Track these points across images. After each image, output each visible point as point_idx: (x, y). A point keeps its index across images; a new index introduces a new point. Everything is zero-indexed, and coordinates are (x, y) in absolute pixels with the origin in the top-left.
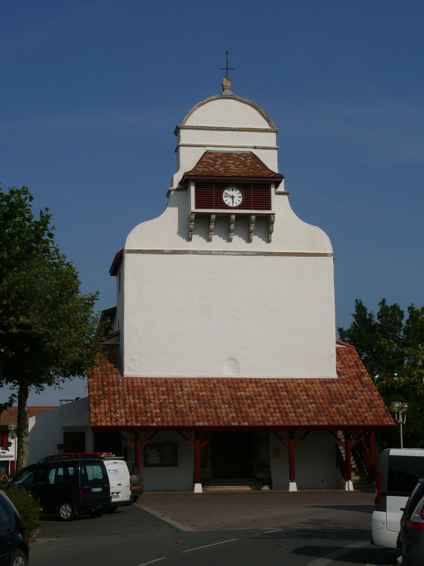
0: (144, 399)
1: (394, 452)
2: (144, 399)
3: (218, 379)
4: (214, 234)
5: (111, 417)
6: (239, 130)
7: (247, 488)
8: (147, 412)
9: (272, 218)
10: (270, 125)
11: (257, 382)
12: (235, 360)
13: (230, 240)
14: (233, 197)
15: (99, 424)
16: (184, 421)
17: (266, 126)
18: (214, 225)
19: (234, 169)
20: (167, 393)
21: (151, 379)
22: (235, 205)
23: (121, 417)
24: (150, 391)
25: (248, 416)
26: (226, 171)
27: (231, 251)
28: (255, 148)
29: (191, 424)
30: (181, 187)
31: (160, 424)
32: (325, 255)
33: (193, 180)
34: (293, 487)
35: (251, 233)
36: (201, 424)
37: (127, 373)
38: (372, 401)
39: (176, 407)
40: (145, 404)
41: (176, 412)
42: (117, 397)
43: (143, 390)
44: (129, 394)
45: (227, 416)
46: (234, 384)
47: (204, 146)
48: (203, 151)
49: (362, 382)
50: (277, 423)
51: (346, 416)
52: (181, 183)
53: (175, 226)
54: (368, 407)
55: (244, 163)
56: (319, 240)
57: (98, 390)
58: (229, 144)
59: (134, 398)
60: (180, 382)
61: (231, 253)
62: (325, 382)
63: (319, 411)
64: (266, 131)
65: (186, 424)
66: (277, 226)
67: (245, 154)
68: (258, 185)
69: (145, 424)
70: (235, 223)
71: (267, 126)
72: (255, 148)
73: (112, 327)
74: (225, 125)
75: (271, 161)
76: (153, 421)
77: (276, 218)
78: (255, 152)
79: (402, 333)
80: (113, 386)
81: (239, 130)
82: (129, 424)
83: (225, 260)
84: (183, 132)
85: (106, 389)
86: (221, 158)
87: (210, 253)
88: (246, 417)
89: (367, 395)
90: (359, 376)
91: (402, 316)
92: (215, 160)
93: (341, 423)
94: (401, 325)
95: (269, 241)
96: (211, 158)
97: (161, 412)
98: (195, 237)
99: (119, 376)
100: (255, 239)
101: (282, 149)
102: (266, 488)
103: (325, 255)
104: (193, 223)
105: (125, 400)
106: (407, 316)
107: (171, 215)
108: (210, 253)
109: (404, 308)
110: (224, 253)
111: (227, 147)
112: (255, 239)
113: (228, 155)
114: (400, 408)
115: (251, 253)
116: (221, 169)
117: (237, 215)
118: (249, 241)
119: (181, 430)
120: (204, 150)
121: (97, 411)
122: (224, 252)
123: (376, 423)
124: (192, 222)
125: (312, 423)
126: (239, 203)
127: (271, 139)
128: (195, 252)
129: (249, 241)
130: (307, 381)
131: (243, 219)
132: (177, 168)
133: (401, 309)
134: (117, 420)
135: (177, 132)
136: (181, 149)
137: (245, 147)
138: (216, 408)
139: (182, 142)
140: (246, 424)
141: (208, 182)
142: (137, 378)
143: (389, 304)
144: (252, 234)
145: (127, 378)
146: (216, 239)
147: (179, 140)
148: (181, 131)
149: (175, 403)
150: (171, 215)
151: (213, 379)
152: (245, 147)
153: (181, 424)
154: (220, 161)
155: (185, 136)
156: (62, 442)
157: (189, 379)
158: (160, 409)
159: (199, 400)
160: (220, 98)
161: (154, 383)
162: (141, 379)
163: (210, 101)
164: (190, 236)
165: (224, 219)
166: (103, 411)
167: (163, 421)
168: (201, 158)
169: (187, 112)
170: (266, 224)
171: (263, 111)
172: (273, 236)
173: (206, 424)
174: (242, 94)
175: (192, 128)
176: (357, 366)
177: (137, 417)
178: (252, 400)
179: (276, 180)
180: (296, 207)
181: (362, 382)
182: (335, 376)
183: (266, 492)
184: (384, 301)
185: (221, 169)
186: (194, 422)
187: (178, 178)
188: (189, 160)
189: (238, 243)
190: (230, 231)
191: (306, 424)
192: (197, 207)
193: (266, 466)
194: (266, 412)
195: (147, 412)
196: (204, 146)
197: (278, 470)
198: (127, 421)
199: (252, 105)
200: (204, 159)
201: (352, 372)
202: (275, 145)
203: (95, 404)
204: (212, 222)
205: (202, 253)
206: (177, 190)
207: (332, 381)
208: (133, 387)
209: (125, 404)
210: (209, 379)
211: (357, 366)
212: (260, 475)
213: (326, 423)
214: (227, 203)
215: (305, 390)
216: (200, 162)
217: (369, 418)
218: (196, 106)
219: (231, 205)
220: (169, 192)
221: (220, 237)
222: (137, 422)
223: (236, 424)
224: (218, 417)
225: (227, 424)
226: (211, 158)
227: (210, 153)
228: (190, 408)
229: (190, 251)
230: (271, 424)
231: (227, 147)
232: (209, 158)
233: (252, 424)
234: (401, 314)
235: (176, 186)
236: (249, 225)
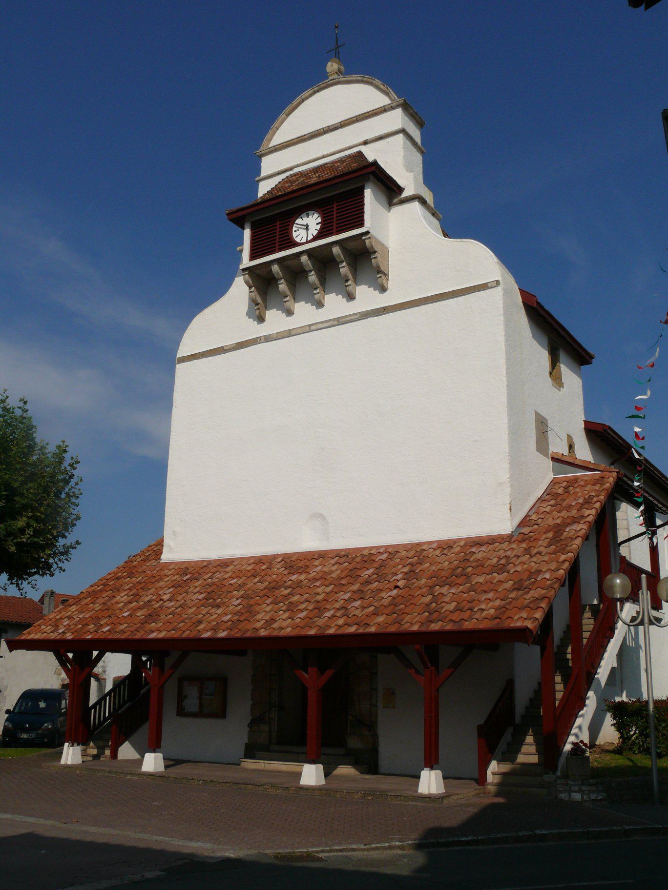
10: (387, 94)
12: (321, 517)
27: (320, 323)
64: (384, 110)
71: (384, 101)
83: (323, 336)
87: (268, 339)
95: (383, 289)
107: (240, 290)
108: (268, 339)
110: (289, 334)
111: (323, 157)
115: (353, 317)
122: (310, 326)
131: (324, 261)
137: (350, 148)
152: (350, 148)
156: (12, 709)
163: (303, 101)
174: (358, 69)
189: (334, 304)
197: (398, 736)
218: (282, 116)
221: (375, 290)
229: (259, 338)
231: (323, 157)
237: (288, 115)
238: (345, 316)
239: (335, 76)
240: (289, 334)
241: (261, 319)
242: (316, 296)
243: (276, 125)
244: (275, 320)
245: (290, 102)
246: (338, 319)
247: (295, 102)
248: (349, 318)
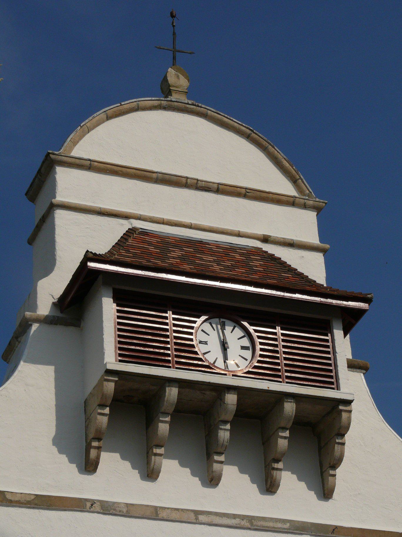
4: (168, 456)
9: (344, 415)
10: (294, 181)
17: (286, 188)
18: (171, 424)
27: (217, 514)
30: (58, 314)
33: (106, 284)
35: (277, 461)
47: (126, 217)
53: (47, 424)
58: (194, 222)
61: (218, 520)
67: (241, 249)
70: (232, 423)
72: (265, 239)
74: (167, 169)
77: (354, 416)
81: (220, 189)
84: (62, 175)
87: (154, 514)
95: (326, 493)
98: (111, 462)
104: (107, 411)
108: (154, 514)
112: (289, 481)
115: (279, 525)
120: (124, 226)
122: (197, 513)
124: (102, 406)
127: (304, 225)
128: (107, 509)
131: (256, 414)
132: (48, 265)
136: (60, 215)
137: (239, 235)
144: (280, 465)
148: (59, 170)
152: (239, 235)
155: (68, 184)
160: (165, 108)
163: (137, 109)
164: (93, 453)
169: (77, 116)
187: (51, 288)
192: (125, 355)
196: (126, 217)
199: (248, 137)
204: (165, 414)
205: (130, 511)
206: (48, 321)
218: (100, 114)
220: (25, 325)
229: (93, 502)
235: (44, 306)
237: (108, 118)
238: (264, 519)
239: (184, 99)
240: (195, 517)
241: (89, 466)
242: (216, 466)
243: (87, 123)
244: (116, 476)
245: (120, 101)
246: (251, 519)
247: (127, 104)
248: (271, 524)
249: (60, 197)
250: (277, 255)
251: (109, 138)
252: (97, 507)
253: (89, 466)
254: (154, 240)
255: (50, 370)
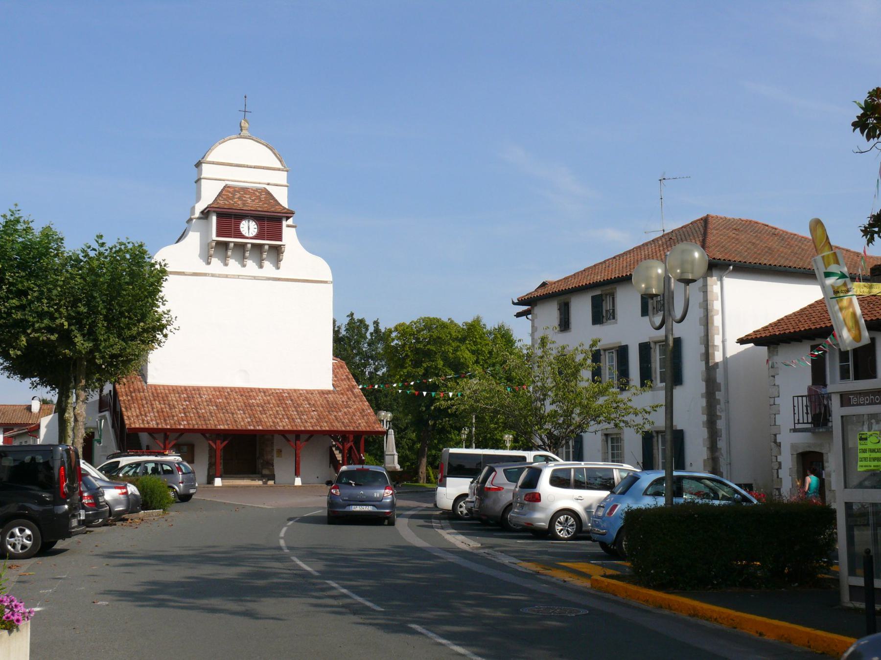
0: (169, 405)
1: (452, 450)
2: (169, 405)
3: (230, 388)
5: (143, 421)
6: (255, 167)
7: (260, 483)
8: (173, 416)
11: (265, 391)
13: (244, 266)
14: (249, 228)
15: (133, 426)
16: (206, 424)
17: (279, 165)
19: (251, 204)
20: (189, 398)
21: (172, 386)
22: (251, 235)
23: (152, 420)
24: (173, 397)
25: (261, 421)
26: (244, 204)
28: (268, 184)
29: (213, 427)
31: (187, 427)
32: (326, 282)
34: (298, 482)
36: (222, 427)
37: (151, 380)
38: (363, 410)
39: (198, 413)
40: (170, 409)
41: (199, 417)
42: (144, 402)
43: (167, 397)
44: (155, 400)
45: (243, 422)
46: (246, 393)
48: (221, 185)
49: (354, 394)
50: (286, 428)
51: (343, 423)
52: (202, 212)
54: (359, 415)
55: (259, 198)
56: (321, 269)
57: (127, 395)
59: (160, 404)
60: (198, 389)
62: (322, 393)
63: (320, 418)
64: (279, 170)
65: (209, 427)
66: (286, 256)
68: (271, 221)
69: (174, 427)
71: (280, 166)
72: (268, 184)
73: (604, 437)
74: (242, 163)
75: (282, 197)
76: (180, 424)
78: (269, 188)
79: (366, 345)
80: (139, 392)
81: (255, 167)
82: (160, 426)
85: (133, 395)
86: (238, 192)
87: (227, 276)
88: (260, 422)
89: (358, 405)
90: (351, 389)
91: (367, 329)
92: (234, 195)
93: (340, 429)
94: (365, 338)
96: (229, 192)
97: (186, 416)
98: (215, 261)
99: (143, 383)
100: (267, 264)
101: (292, 187)
102: (271, 483)
103: (326, 282)
105: (152, 405)
106: (371, 329)
108: (227, 276)
109: (369, 322)
110: (239, 277)
112: (267, 264)
113: (245, 190)
114: (385, 416)
116: (240, 202)
117: (253, 245)
118: (261, 267)
119: (204, 432)
121: (130, 414)
123: (368, 429)
125: (316, 428)
126: (254, 234)
127: (282, 177)
128: (213, 275)
129: (261, 267)
130: (308, 391)
132: (198, 198)
133: (367, 323)
134: (148, 423)
135: (198, 165)
138: (233, 414)
139: (202, 176)
140: (261, 428)
141: (227, 216)
142: (159, 386)
143: (357, 317)
145: (151, 385)
146: (232, 262)
147: (200, 172)
149: (196, 409)
150: (194, 239)
151: (226, 388)
153: (205, 427)
154: (238, 195)
157: (206, 387)
158: (185, 413)
159: (217, 406)
161: (175, 390)
162: (163, 386)
165: (241, 247)
166: (134, 414)
167: (189, 424)
168: (222, 190)
170: (277, 251)
171: (276, 151)
172: (282, 263)
173: (226, 427)
175: (213, 163)
176: (349, 379)
177: (165, 420)
178: (262, 407)
179: (288, 214)
180: (301, 237)
181: (354, 394)
182: (331, 388)
183: (271, 486)
184: (352, 314)
185: (240, 202)
186: (215, 425)
187: (200, 207)
188: (209, 194)
190: (244, 258)
191: (311, 429)
192: (218, 236)
193: (270, 464)
194: (276, 418)
195: (173, 416)
198: (157, 424)
200: (224, 193)
201: (345, 385)
202: (285, 183)
203: (126, 408)
205: (220, 276)
206: (199, 218)
207: (329, 392)
208: (157, 394)
209: (153, 409)
210: (223, 388)
211: (349, 379)
212: (266, 472)
213: (327, 429)
214: (244, 233)
215: (307, 399)
216: (220, 195)
217: (363, 426)
219: (247, 235)
220: (191, 220)
222: (166, 424)
223: (252, 428)
224: (236, 421)
225: (244, 428)
226: (229, 192)
227: (229, 187)
228: (211, 413)
230: (281, 428)
232: (227, 191)
233: (266, 428)
234: (367, 327)
235: (197, 214)
236: (261, 253)
249: (202, 176)
250: (67, 540)
251: (219, 153)
252: (144, 438)
253: (209, 263)
254: (231, 190)
255: (198, 234)
